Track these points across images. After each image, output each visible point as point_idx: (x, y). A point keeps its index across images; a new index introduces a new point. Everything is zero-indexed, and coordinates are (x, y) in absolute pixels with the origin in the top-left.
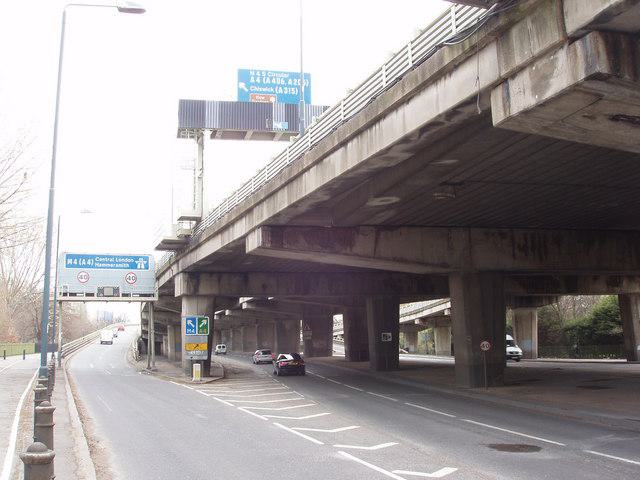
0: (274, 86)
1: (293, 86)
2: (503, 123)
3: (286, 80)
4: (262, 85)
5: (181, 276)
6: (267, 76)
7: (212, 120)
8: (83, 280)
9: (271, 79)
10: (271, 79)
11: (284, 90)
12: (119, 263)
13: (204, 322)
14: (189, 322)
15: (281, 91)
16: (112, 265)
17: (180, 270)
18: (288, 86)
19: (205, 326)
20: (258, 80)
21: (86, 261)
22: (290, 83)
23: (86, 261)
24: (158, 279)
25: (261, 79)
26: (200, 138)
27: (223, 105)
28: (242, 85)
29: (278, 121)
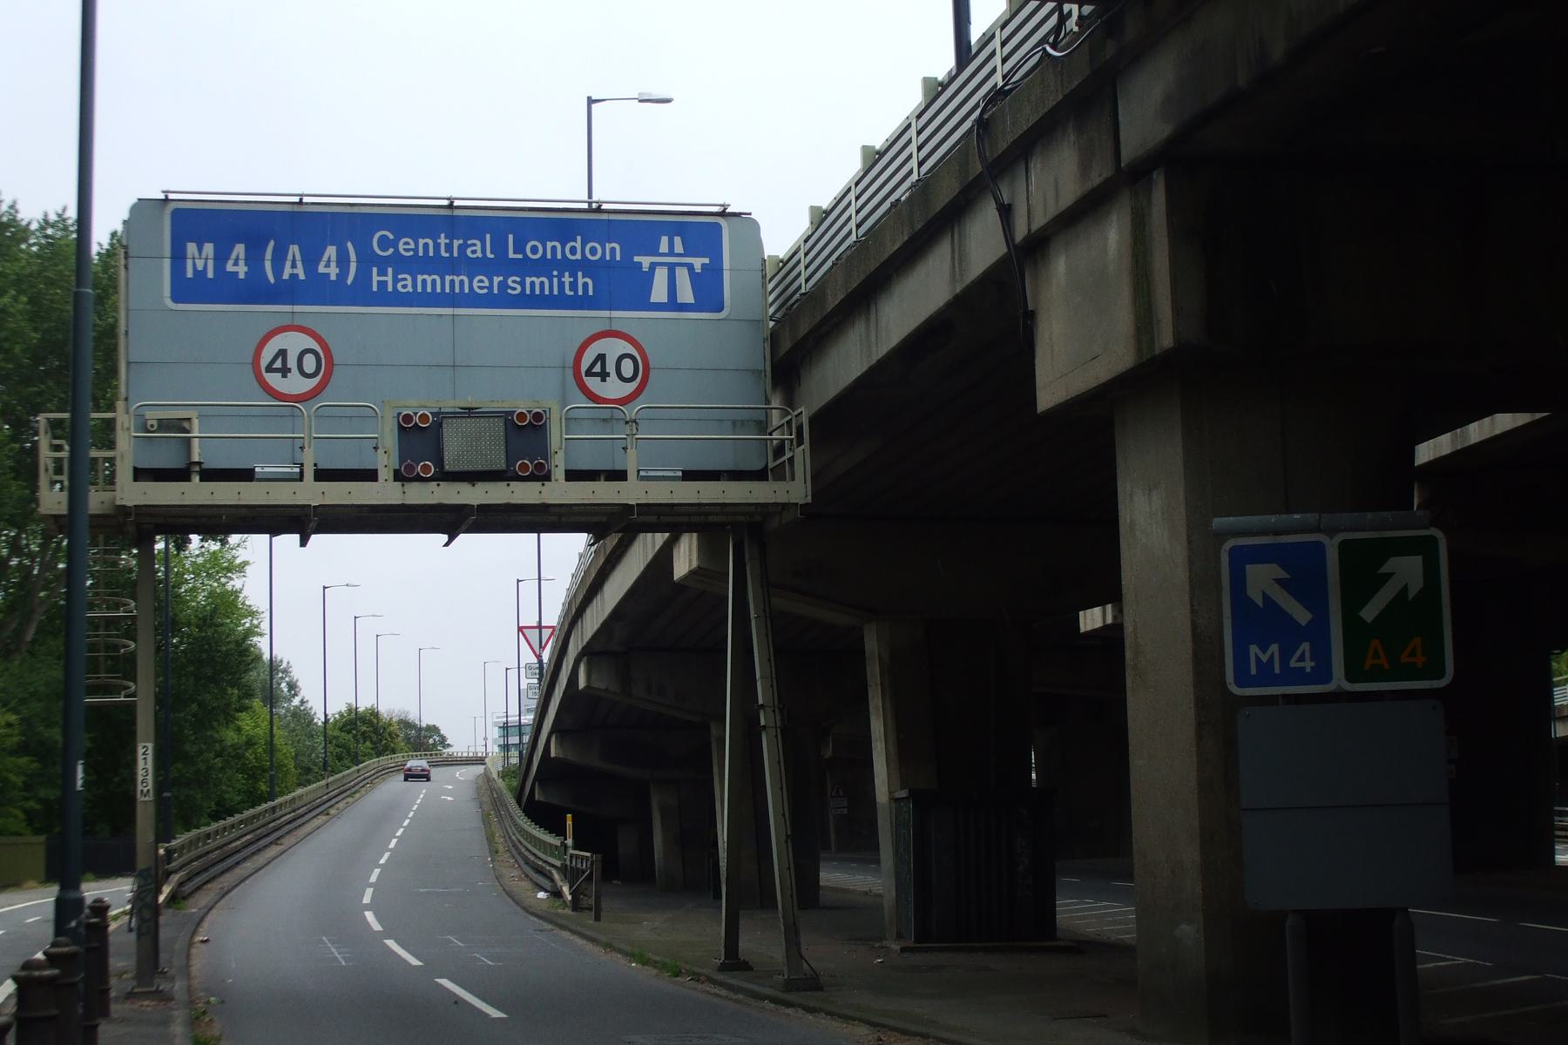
12: (525, 267)
16: (480, 284)
21: (311, 260)
23: (311, 260)
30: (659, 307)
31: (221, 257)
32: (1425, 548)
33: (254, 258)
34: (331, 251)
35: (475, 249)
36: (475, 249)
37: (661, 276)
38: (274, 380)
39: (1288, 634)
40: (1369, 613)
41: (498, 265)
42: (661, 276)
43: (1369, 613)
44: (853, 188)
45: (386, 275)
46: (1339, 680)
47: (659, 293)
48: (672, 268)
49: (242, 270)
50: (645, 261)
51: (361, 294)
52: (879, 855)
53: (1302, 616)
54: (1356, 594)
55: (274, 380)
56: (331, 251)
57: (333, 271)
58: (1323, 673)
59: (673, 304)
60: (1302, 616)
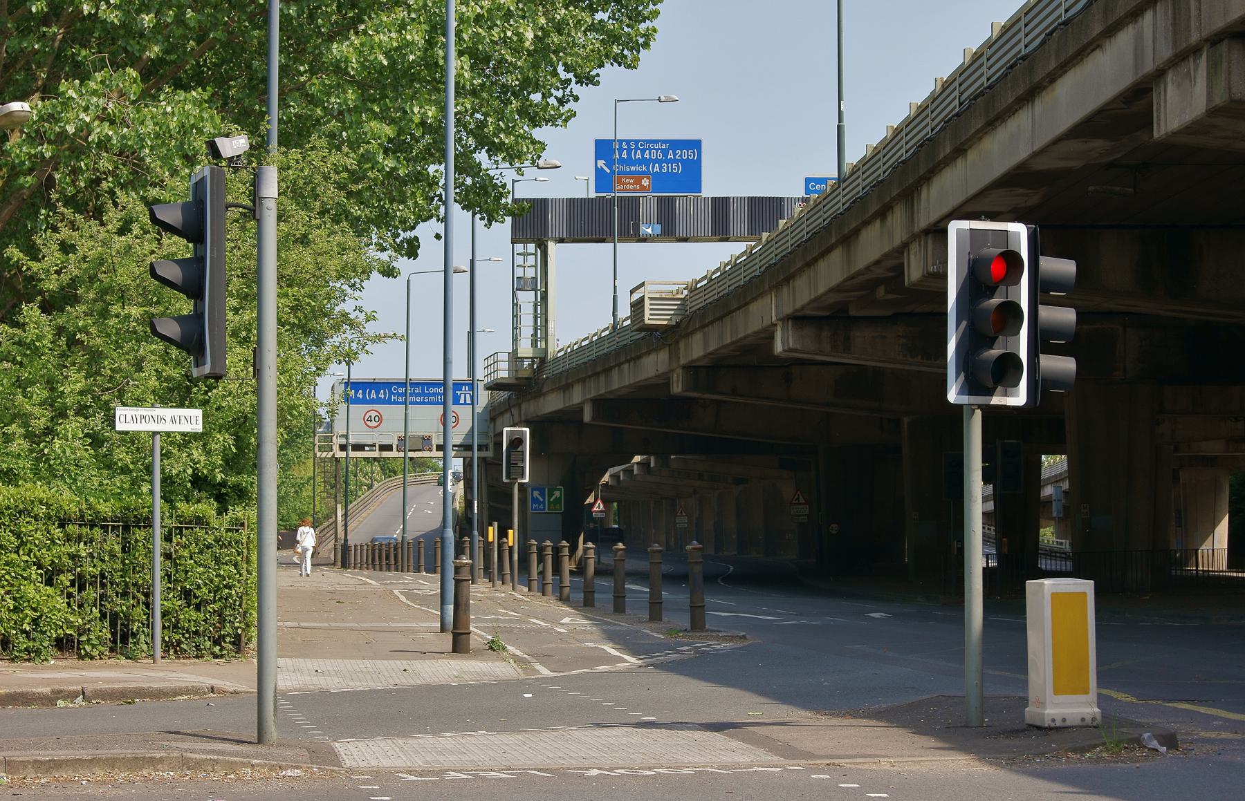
0: (646, 162)
1: (675, 161)
2: (1187, 130)
3: (665, 152)
4: (628, 161)
5: (680, 371)
6: (637, 149)
7: (556, 222)
8: (373, 424)
9: (643, 152)
10: (643, 152)
11: (661, 168)
12: (429, 395)
13: (557, 494)
14: (536, 493)
15: (657, 169)
16: (418, 399)
17: (523, 419)
18: (668, 161)
19: (557, 500)
20: (625, 155)
21: (377, 393)
22: (670, 155)
23: (377, 393)
24: (632, 292)
25: (629, 153)
26: (542, 246)
27: (572, 203)
28: (601, 163)
29: (649, 223)
30: (462, 404)
31: (356, 393)
32: (560, 490)
33: (364, 393)
34: (382, 391)
35: (417, 390)
36: (417, 390)
37: (463, 396)
38: (368, 423)
39: (540, 503)
40: (551, 500)
41: (422, 394)
42: (463, 396)
43: (551, 500)
44: (1023, 17)
45: (279, 629)
46: (547, 511)
47: (462, 401)
48: (465, 394)
49: (361, 396)
50: (459, 393)
51: (389, 402)
52: (1025, 684)
53: (542, 500)
54: (550, 497)
55: (368, 423)
56: (382, 391)
57: (383, 396)
58: (544, 509)
59: (465, 403)
60: (542, 500)
